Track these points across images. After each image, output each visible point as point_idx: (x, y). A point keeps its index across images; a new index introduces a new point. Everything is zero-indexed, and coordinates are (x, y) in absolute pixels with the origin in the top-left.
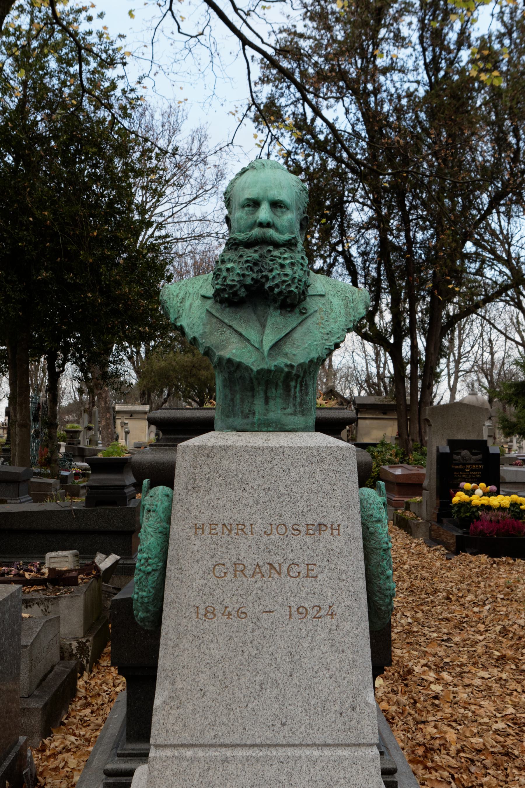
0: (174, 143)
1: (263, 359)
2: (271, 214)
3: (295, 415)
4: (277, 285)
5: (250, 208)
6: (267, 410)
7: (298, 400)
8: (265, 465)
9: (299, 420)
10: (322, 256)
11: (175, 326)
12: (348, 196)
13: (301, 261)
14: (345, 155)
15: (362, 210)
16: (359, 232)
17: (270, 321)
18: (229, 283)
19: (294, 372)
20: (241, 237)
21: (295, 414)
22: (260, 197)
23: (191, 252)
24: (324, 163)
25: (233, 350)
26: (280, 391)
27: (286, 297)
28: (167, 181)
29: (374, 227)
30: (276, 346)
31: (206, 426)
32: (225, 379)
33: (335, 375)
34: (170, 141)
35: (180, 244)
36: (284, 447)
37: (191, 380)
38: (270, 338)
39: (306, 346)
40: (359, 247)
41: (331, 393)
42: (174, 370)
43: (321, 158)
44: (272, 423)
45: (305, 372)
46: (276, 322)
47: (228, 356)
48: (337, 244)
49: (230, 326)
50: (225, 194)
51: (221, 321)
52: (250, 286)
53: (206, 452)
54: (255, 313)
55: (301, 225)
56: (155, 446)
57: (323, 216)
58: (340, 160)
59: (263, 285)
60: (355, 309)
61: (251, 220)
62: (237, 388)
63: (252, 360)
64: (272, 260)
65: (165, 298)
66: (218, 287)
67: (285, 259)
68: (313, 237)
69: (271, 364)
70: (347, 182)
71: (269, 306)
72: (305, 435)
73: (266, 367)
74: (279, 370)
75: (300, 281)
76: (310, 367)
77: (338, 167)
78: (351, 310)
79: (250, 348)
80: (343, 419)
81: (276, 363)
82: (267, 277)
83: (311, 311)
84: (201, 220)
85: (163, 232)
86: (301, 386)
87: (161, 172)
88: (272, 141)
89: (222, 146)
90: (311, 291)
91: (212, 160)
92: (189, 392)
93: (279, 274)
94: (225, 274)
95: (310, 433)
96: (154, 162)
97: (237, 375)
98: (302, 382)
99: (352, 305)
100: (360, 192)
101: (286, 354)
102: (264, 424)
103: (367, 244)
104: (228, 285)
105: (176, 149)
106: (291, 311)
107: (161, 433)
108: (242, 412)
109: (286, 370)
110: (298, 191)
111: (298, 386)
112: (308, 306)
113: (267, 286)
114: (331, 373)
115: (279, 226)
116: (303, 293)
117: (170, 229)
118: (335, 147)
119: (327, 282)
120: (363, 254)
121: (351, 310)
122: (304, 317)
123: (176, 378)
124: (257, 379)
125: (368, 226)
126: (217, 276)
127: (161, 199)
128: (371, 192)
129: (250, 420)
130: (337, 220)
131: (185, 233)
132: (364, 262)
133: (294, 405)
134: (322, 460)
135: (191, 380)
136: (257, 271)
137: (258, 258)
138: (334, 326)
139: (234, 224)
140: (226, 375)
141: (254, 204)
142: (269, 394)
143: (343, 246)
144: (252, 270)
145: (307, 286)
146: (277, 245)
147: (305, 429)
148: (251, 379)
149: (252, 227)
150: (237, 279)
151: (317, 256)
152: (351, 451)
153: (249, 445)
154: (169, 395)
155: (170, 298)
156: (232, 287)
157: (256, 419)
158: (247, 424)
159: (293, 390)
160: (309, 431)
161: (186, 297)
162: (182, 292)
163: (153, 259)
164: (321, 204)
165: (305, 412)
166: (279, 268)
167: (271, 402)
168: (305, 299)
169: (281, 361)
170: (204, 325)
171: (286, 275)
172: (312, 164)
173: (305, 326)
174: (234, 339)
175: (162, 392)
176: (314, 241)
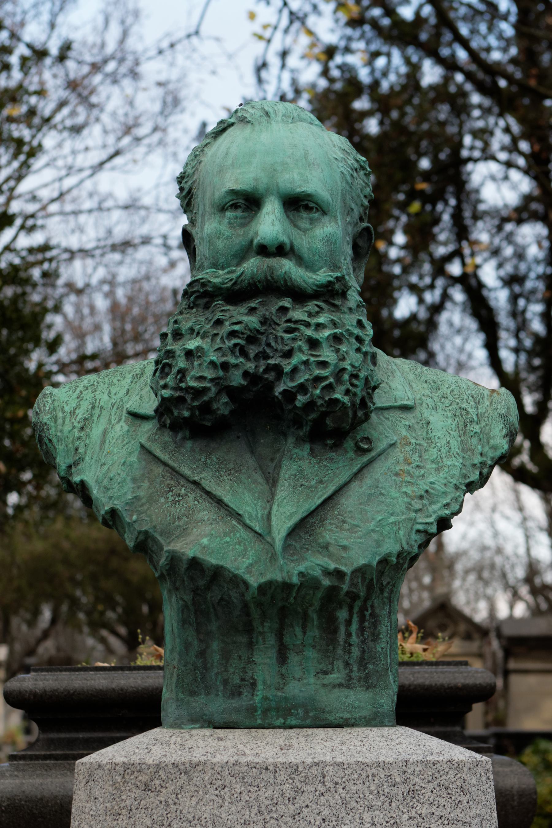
0: (63, 32)
1: (273, 558)
2: (287, 224)
3: (349, 687)
4: (302, 389)
5: (239, 213)
6: (283, 676)
7: (356, 652)
8: (281, 808)
9: (358, 699)
10: (414, 289)
11: (69, 483)
12: (472, 148)
13: (356, 331)
14: (462, 55)
15: (506, 178)
16: (500, 228)
17: (288, 470)
18: (192, 384)
19: (345, 587)
20: (218, 277)
21: (348, 684)
22: (261, 187)
23: (103, 282)
24: (414, 70)
25: (203, 539)
26: (314, 632)
27: (324, 415)
28: (47, 121)
29: (535, 217)
30: (303, 528)
31: (138, 713)
32: (186, 606)
33: (451, 567)
34: (52, 26)
35: (78, 264)
36: (325, 764)
37: (107, 584)
38: (288, 509)
39: (372, 526)
40: (500, 266)
41: (443, 617)
42: (66, 561)
43: (407, 61)
44: (296, 707)
45: (370, 588)
46: (300, 471)
47: (190, 554)
48: (448, 258)
49: (195, 483)
50: (181, 179)
51: (175, 472)
52: (241, 389)
53: (144, 778)
54: (252, 452)
55: (355, 247)
56: (23, 758)
57: (413, 195)
58: (450, 65)
59: (271, 386)
60: (484, 437)
61: (239, 239)
62: (214, 626)
63: (248, 561)
64: (289, 331)
65: (45, 418)
66: (166, 393)
67: (319, 326)
68: (391, 243)
69: (291, 570)
70: (469, 115)
71: (285, 435)
72: (373, 733)
73: (278, 577)
74: (308, 583)
75: (356, 376)
76: (381, 573)
77: (447, 79)
78: (474, 441)
79: (242, 532)
80: (465, 687)
81: (302, 568)
82: (278, 370)
83: (381, 446)
84: (126, 207)
85: (38, 239)
86: (362, 619)
87: (33, 100)
88: (291, 22)
89: (174, 39)
90: (380, 399)
91: (152, 70)
92: (102, 613)
93: (306, 363)
94: (181, 363)
95: (386, 730)
96: (17, 75)
97: (214, 595)
98: (363, 609)
99: (477, 428)
100: (500, 139)
101: (326, 547)
102: (277, 710)
103: (520, 255)
104: (188, 389)
105: (66, 48)
106: (337, 446)
107: (35, 727)
108: (225, 682)
109: (326, 582)
110: (346, 170)
111: (355, 619)
112: (374, 435)
113: (279, 389)
114: (443, 565)
115: (305, 253)
116: (363, 404)
117: (57, 232)
118: (437, 36)
119: (418, 377)
120: (513, 281)
121: (474, 441)
122: (365, 458)
123: (72, 579)
124: (260, 605)
125: (522, 213)
126: (163, 367)
127: (32, 161)
128: (525, 136)
129: (244, 701)
130: (446, 203)
131: (89, 238)
132: (514, 298)
133: (347, 664)
134: (413, 792)
135: (107, 584)
136: (257, 357)
137: (257, 326)
138: (436, 480)
139: (202, 249)
140: (188, 598)
141: (248, 202)
142: (287, 639)
143: (464, 264)
144: (243, 353)
145: (371, 387)
146: (300, 296)
148: (246, 606)
149: (242, 255)
150: (209, 374)
151: (399, 288)
152: (480, 770)
153: (243, 760)
154: (54, 621)
155: (55, 420)
156: (198, 393)
157: (257, 699)
158: (238, 711)
159: (342, 629)
160: (382, 724)
161: (96, 422)
162: (85, 405)
163: (15, 299)
164: (409, 167)
165: (373, 680)
166: (305, 348)
167: (294, 659)
168: (367, 417)
169: (314, 563)
170: (134, 480)
171: (324, 364)
172: (385, 74)
173: (368, 480)
174: (206, 512)
175: (36, 613)
176: (394, 253)
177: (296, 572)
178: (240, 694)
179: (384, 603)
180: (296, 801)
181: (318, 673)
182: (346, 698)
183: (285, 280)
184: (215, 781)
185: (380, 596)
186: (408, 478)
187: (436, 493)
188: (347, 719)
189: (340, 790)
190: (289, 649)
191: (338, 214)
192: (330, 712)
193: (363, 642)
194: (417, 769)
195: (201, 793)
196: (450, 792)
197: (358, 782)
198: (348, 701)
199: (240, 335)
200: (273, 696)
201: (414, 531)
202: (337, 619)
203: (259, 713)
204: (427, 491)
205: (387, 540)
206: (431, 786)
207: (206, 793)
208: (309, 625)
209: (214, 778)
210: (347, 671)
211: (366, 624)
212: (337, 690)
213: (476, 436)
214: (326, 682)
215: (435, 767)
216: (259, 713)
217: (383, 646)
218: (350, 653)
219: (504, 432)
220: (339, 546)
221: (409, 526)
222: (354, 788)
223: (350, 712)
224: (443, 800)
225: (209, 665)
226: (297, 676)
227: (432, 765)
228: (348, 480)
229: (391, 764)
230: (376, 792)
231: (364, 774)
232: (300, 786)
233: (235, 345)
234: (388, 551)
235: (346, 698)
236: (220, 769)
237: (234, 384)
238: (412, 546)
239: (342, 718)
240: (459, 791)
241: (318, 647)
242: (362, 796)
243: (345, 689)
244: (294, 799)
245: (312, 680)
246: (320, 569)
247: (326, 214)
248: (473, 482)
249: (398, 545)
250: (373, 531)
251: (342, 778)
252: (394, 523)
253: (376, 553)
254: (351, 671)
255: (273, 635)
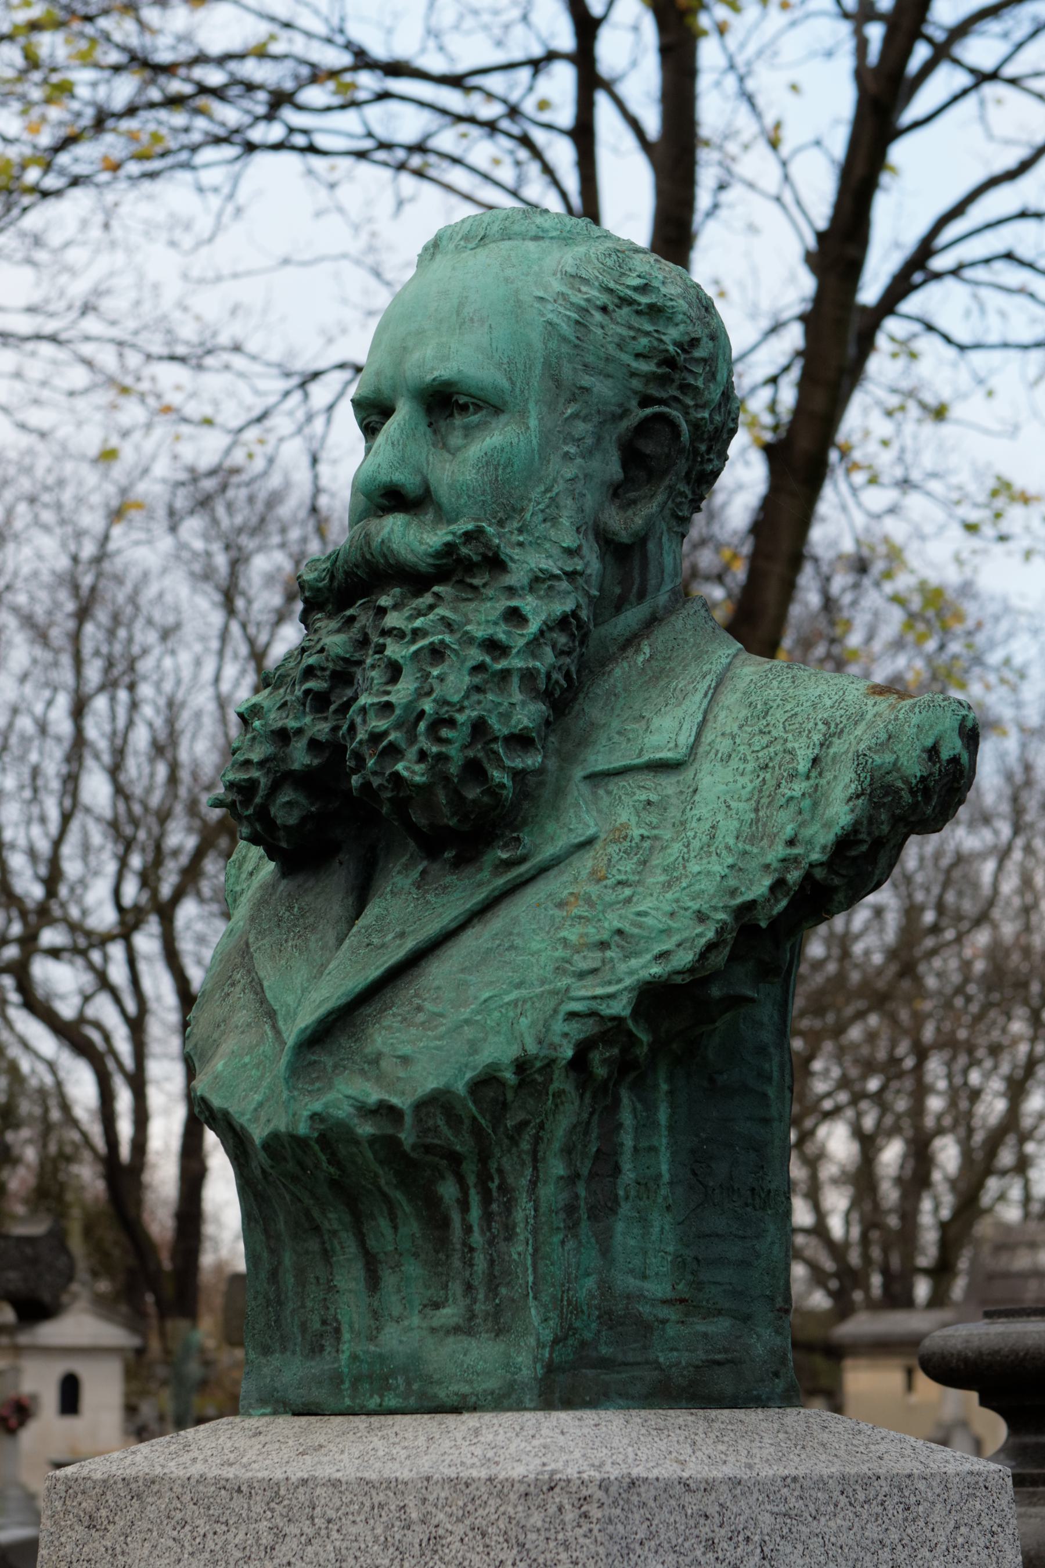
6: (376, 1314)
7: (481, 1262)
9: (480, 1356)
21: (466, 1329)
26: (412, 1227)
39: (465, 1013)
44: (392, 1374)
74: (330, 1136)
81: (317, 1106)
86: (487, 1199)
101: (376, 1060)
109: (366, 1129)
133: (469, 1288)
142: (371, 1243)
146: (415, 580)
147: (503, 1400)
157: (344, 1357)
159: (456, 1217)
167: (389, 1280)
177: (306, 1113)
178: (322, 1348)
179: (523, 1164)
180: (274, 1553)
181: (425, 1306)
182: (465, 1355)
183: (385, 556)
184: (173, 1513)
185: (514, 1150)
186: (582, 910)
187: (645, 933)
188: (464, 1396)
189: (335, 1535)
190: (381, 1262)
191: (531, 405)
192: (439, 1382)
193: (491, 1243)
194: (443, 1495)
195: (155, 1534)
196: (488, 1541)
197: (358, 1520)
198: (469, 1360)
199: (319, 673)
200: (364, 1352)
201: (561, 1016)
202: (441, 1198)
203: (347, 1385)
204: (620, 932)
205: (492, 1038)
206: (460, 1529)
207: (161, 1536)
208: (399, 1213)
209: (171, 1507)
210: (468, 1301)
211: (494, 1206)
212: (451, 1339)
213: (792, 804)
214: (435, 1323)
215: (467, 1491)
216: (347, 1385)
217: (520, 1249)
218: (472, 1265)
219: (852, 789)
220: (398, 1057)
221: (552, 1004)
222: (354, 1530)
223: (470, 1382)
224: (478, 1558)
225: (283, 1297)
226: (395, 1313)
227: (463, 1487)
228: (453, 925)
229: (406, 1484)
230: (382, 1539)
231: (368, 1504)
232: (281, 1525)
233: (307, 692)
234: (490, 1060)
235: (465, 1355)
236: (180, 1490)
237: (296, 766)
238: (554, 1047)
239: (456, 1394)
240: (501, 1539)
241: (423, 1256)
242: (363, 1546)
243: (464, 1337)
244: (273, 1548)
245: (416, 1320)
246: (352, 1105)
247: (503, 411)
248: (754, 902)
249: (515, 1047)
250: (467, 1022)
251: (338, 1510)
252: (515, 1003)
253: (466, 1066)
254: (474, 1301)
255: (350, 1234)
